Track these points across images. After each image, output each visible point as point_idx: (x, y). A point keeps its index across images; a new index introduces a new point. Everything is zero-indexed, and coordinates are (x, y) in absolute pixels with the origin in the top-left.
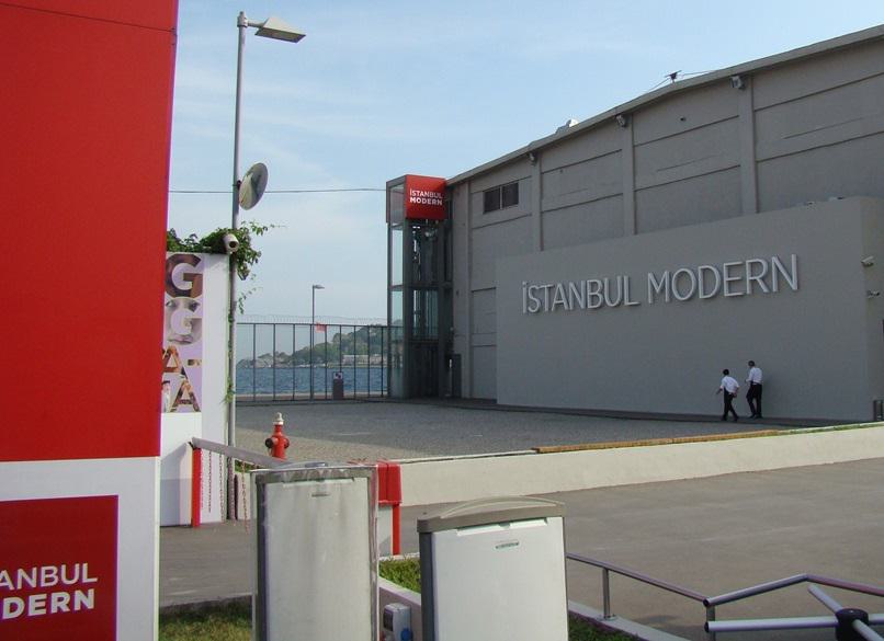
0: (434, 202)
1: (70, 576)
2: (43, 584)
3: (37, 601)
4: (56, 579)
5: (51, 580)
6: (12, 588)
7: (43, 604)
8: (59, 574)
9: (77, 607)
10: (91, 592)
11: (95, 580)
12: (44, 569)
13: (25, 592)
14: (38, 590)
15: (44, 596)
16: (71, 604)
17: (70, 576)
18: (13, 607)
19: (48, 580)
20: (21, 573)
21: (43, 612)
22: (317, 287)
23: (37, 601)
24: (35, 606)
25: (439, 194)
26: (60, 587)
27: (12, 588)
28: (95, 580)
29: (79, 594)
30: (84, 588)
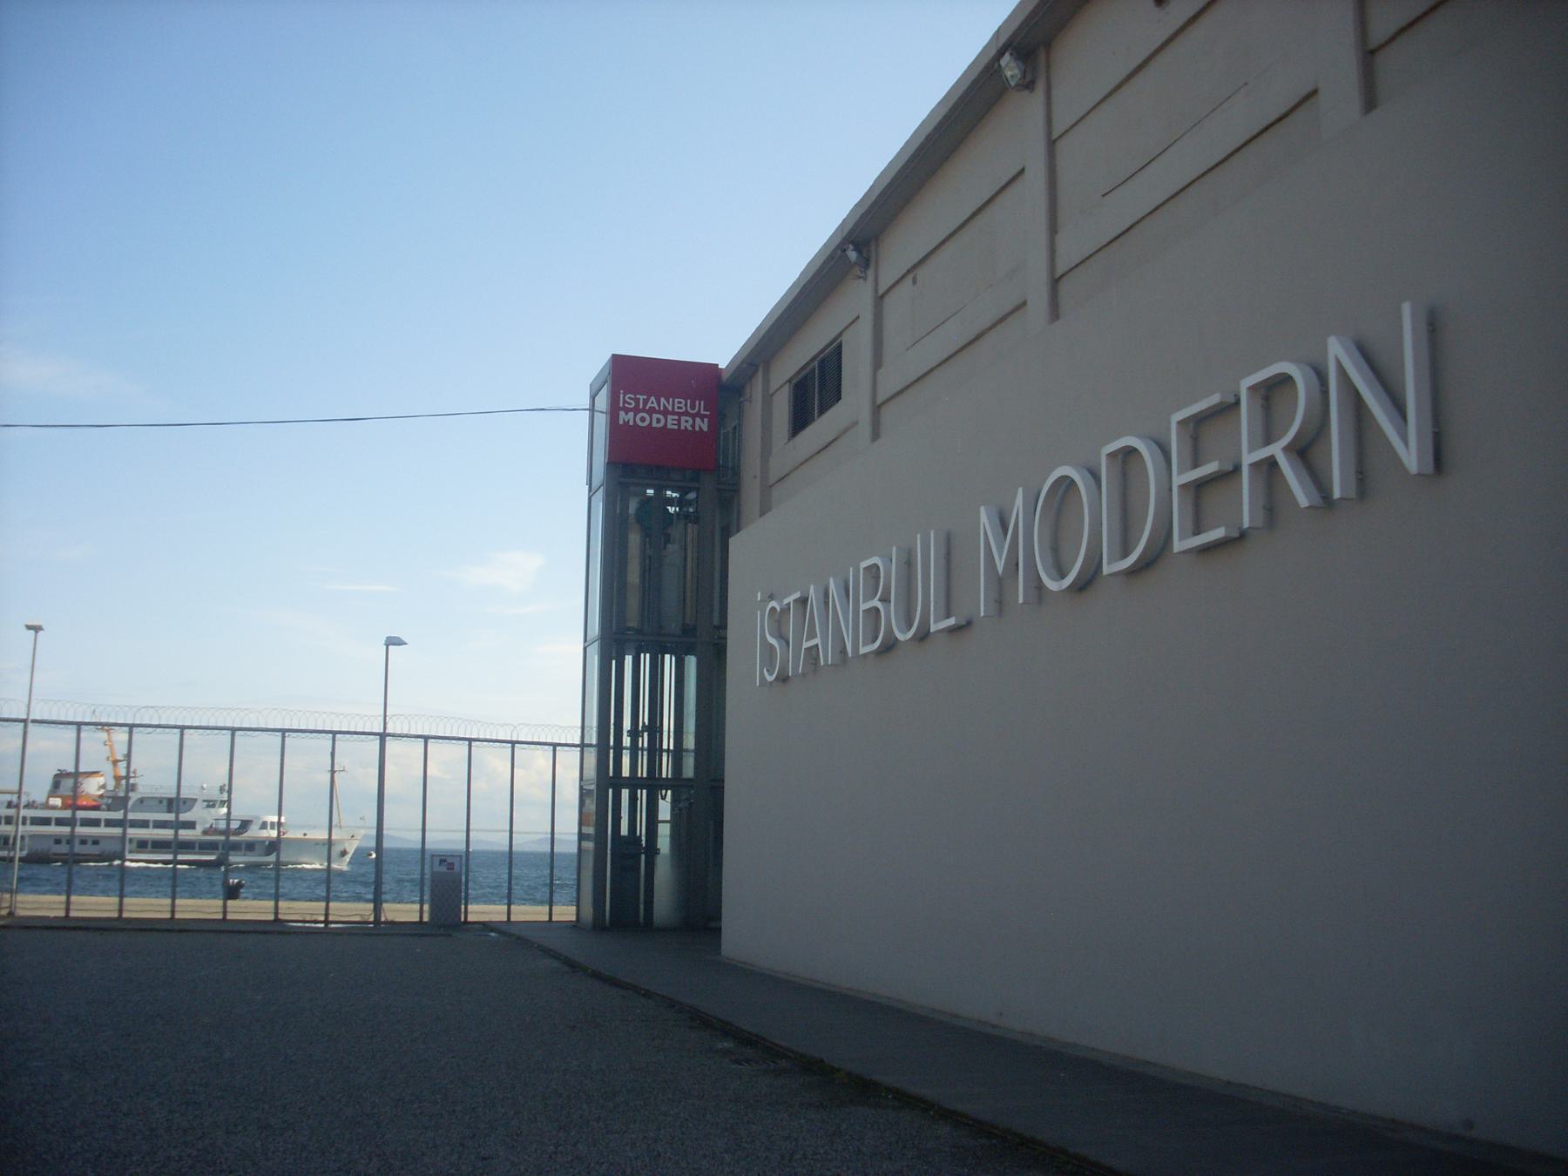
0: (686, 423)
1: (693, 407)
2: (676, 410)
3: (673, 420)
4: (684, 409)
5: (681, 408)
6: (657, 408)
7: (675, 422)
8: (686, 405)
9: (683, 428)
10: (706, 420)
11: (708, 413)
12: (676, 400)
13: (666, 413)
14: (673, 413)
15: (676, 417)
16: (693, 426)
17: (693, 407)
18: (658, 421)
19: (679, 408)
20: (663, 400)
21: (676, 427)
22: (392, 642)
23: (673, 420)
24: (671, 423)
25: (700, 405)
26: (686, 413)
27: (657, 408)
28: (708, 413)
29: (698, 420)
30: (702, 417)
